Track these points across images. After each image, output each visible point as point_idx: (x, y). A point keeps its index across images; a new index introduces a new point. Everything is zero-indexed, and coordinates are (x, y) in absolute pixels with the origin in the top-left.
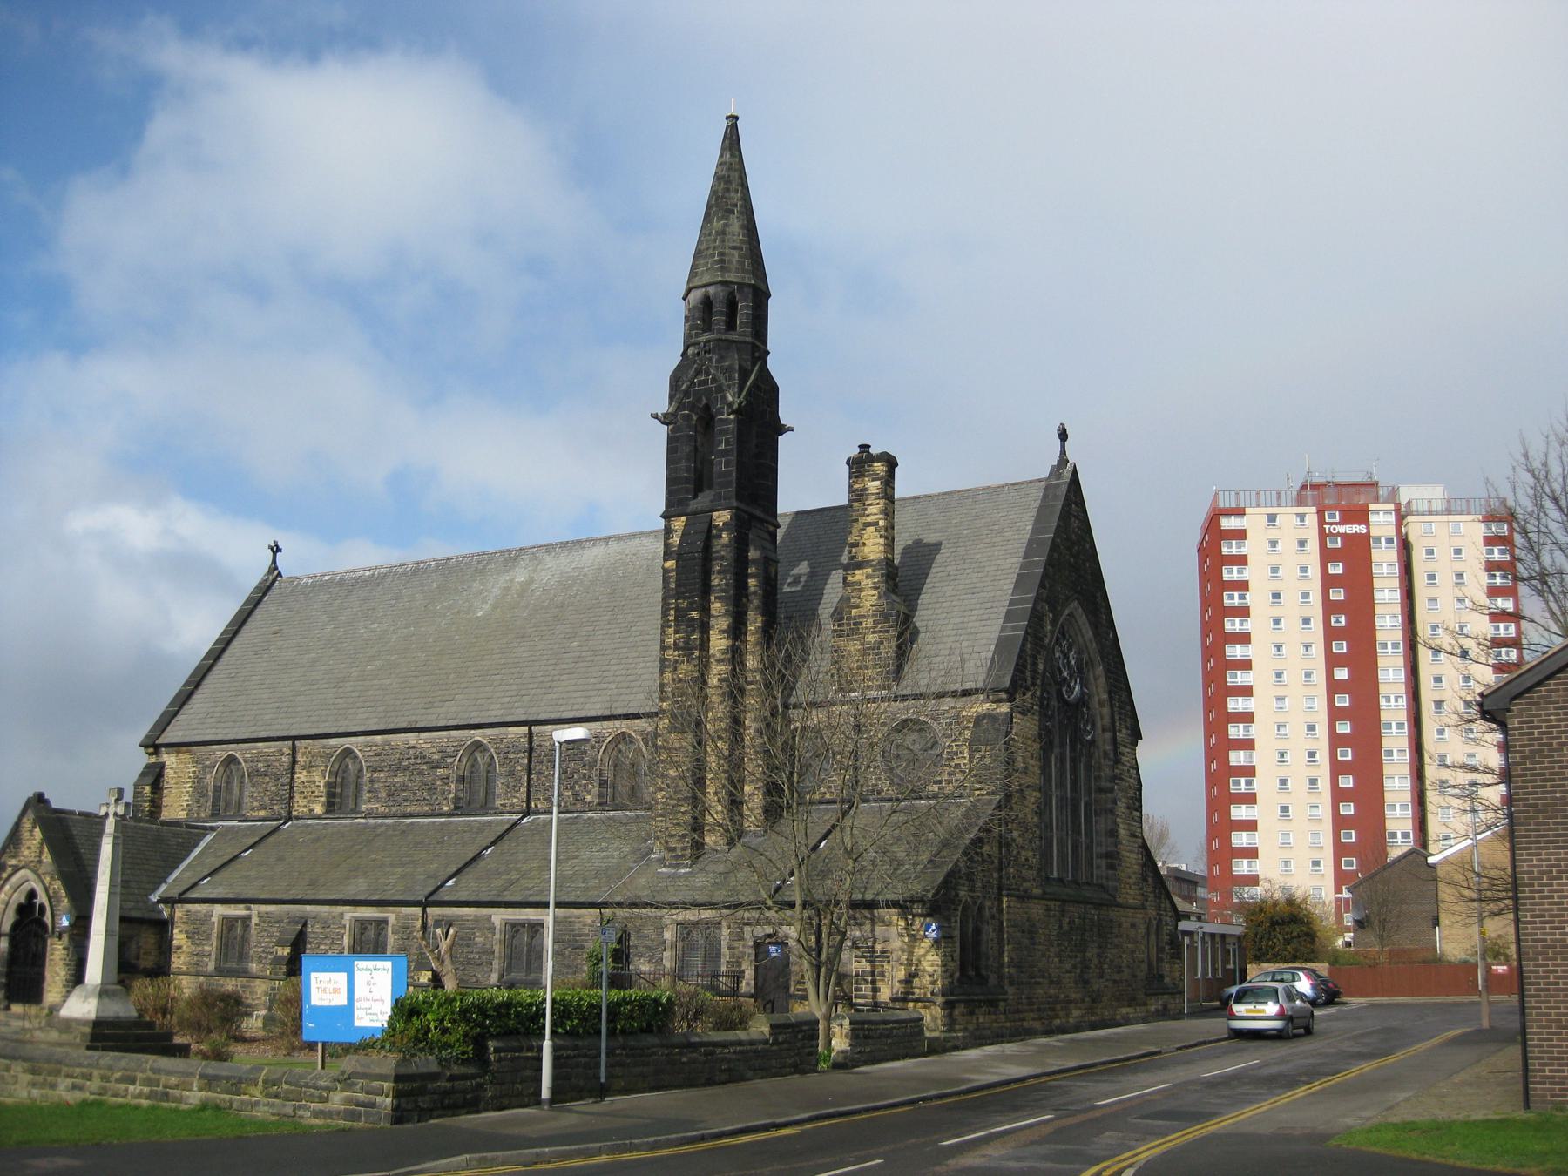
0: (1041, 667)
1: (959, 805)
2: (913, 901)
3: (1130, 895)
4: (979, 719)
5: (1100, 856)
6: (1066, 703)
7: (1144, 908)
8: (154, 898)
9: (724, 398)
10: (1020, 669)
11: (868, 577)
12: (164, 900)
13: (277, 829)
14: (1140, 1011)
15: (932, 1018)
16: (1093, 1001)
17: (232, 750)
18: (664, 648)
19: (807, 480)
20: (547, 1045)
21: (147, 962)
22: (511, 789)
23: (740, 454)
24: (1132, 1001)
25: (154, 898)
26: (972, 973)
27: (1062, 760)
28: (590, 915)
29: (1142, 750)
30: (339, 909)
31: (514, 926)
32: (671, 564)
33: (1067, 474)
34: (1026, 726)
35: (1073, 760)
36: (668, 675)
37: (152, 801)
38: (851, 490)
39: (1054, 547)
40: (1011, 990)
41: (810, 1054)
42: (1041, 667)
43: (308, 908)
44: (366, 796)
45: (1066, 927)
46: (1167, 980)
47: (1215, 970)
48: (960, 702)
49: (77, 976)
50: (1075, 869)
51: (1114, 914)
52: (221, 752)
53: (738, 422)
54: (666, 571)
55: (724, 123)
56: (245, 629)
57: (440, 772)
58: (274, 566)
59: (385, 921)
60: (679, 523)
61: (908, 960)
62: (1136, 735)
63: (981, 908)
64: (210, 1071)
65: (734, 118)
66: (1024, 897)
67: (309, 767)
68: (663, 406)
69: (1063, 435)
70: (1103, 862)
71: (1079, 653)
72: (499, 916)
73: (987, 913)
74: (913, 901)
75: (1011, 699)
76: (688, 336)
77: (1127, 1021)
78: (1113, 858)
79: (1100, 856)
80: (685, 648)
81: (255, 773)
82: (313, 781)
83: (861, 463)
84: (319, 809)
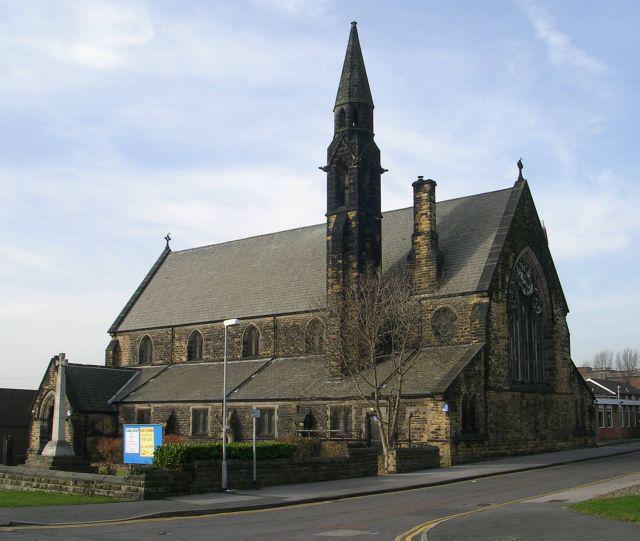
0: (507, 280)
1: (465, 348)
2: (436, 394)
3: (563, 387)
4: (475, 305)
5: (546, 370)
6: (526, 296)
7: (572, 394)
8: (109, 402)
9: (351, 158)
10: (494, 280)
11: (423, 239)
12: (114, 403)
13: (165, 370)
14: (570, 444)
15: (445, 451)
16: (541, 440)
17: (147, 333)
18: (328, 278)
19: (395, 196)
20: (224, 463)
21: (108, 431)
22: (267, 346)
23: (360, 184)
24: (565, 439)
25: (109, 402)
26: (469, 427)
27: (523, 324)
28: (294, 405)
29: (569, 317)
30: (249, 404)
31: (263, 411)
32: (330, 237)
33: (523, 184)
34: (499, 309)
35: (530, 324)
36: (330, 290)
37: (113, 358)
38: (415, 199)
39: (514, 221)
40: (492, 436)
41: (373, 467)
42: (507, 280)
43: (175, 405)
44: (204, 352)
45: (524, 405)
46: (587, 429)
47: (632, 423)
48: (465, 299)
49: (46, 436)
50: (532, 376)
51: (553, 397)
52: (142, 335)
53: (358, 169)
54: (328, 241)
55: (351, 26)
56: (156, 275)
57: (236, 340)
58: (168, 247)
59: (207, 410)
60: (333, 219)
61: (435, 421)
62: (566, 310)
63: (475, 396)
64: (75, 477)
65: (354, 24)
66: (499, 390)
67: (180, 339)
68: (325, 163)
69: (520, 165)
70: (548, 373)
71: (533, 271)
72: (255, 405)
73: (478, 399)
74: (436, 394)
75: (490, 295)
76: (336, 129)
77: (562, 449)
78: (552, 371)
79: (546, 370)
80: (336, 277)
81: (157, 343)
82: (182, 345)
83: (419, 185)
84: (184, 359)
